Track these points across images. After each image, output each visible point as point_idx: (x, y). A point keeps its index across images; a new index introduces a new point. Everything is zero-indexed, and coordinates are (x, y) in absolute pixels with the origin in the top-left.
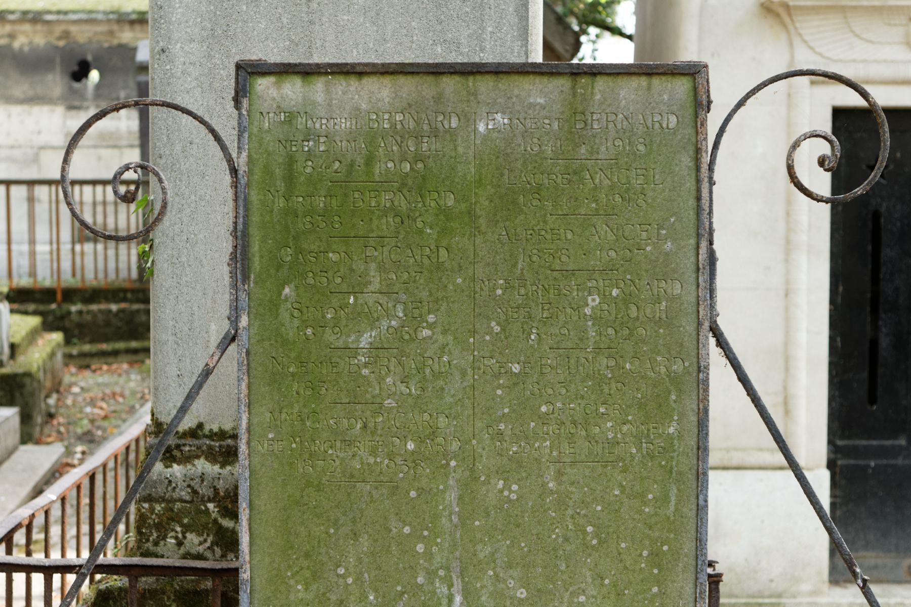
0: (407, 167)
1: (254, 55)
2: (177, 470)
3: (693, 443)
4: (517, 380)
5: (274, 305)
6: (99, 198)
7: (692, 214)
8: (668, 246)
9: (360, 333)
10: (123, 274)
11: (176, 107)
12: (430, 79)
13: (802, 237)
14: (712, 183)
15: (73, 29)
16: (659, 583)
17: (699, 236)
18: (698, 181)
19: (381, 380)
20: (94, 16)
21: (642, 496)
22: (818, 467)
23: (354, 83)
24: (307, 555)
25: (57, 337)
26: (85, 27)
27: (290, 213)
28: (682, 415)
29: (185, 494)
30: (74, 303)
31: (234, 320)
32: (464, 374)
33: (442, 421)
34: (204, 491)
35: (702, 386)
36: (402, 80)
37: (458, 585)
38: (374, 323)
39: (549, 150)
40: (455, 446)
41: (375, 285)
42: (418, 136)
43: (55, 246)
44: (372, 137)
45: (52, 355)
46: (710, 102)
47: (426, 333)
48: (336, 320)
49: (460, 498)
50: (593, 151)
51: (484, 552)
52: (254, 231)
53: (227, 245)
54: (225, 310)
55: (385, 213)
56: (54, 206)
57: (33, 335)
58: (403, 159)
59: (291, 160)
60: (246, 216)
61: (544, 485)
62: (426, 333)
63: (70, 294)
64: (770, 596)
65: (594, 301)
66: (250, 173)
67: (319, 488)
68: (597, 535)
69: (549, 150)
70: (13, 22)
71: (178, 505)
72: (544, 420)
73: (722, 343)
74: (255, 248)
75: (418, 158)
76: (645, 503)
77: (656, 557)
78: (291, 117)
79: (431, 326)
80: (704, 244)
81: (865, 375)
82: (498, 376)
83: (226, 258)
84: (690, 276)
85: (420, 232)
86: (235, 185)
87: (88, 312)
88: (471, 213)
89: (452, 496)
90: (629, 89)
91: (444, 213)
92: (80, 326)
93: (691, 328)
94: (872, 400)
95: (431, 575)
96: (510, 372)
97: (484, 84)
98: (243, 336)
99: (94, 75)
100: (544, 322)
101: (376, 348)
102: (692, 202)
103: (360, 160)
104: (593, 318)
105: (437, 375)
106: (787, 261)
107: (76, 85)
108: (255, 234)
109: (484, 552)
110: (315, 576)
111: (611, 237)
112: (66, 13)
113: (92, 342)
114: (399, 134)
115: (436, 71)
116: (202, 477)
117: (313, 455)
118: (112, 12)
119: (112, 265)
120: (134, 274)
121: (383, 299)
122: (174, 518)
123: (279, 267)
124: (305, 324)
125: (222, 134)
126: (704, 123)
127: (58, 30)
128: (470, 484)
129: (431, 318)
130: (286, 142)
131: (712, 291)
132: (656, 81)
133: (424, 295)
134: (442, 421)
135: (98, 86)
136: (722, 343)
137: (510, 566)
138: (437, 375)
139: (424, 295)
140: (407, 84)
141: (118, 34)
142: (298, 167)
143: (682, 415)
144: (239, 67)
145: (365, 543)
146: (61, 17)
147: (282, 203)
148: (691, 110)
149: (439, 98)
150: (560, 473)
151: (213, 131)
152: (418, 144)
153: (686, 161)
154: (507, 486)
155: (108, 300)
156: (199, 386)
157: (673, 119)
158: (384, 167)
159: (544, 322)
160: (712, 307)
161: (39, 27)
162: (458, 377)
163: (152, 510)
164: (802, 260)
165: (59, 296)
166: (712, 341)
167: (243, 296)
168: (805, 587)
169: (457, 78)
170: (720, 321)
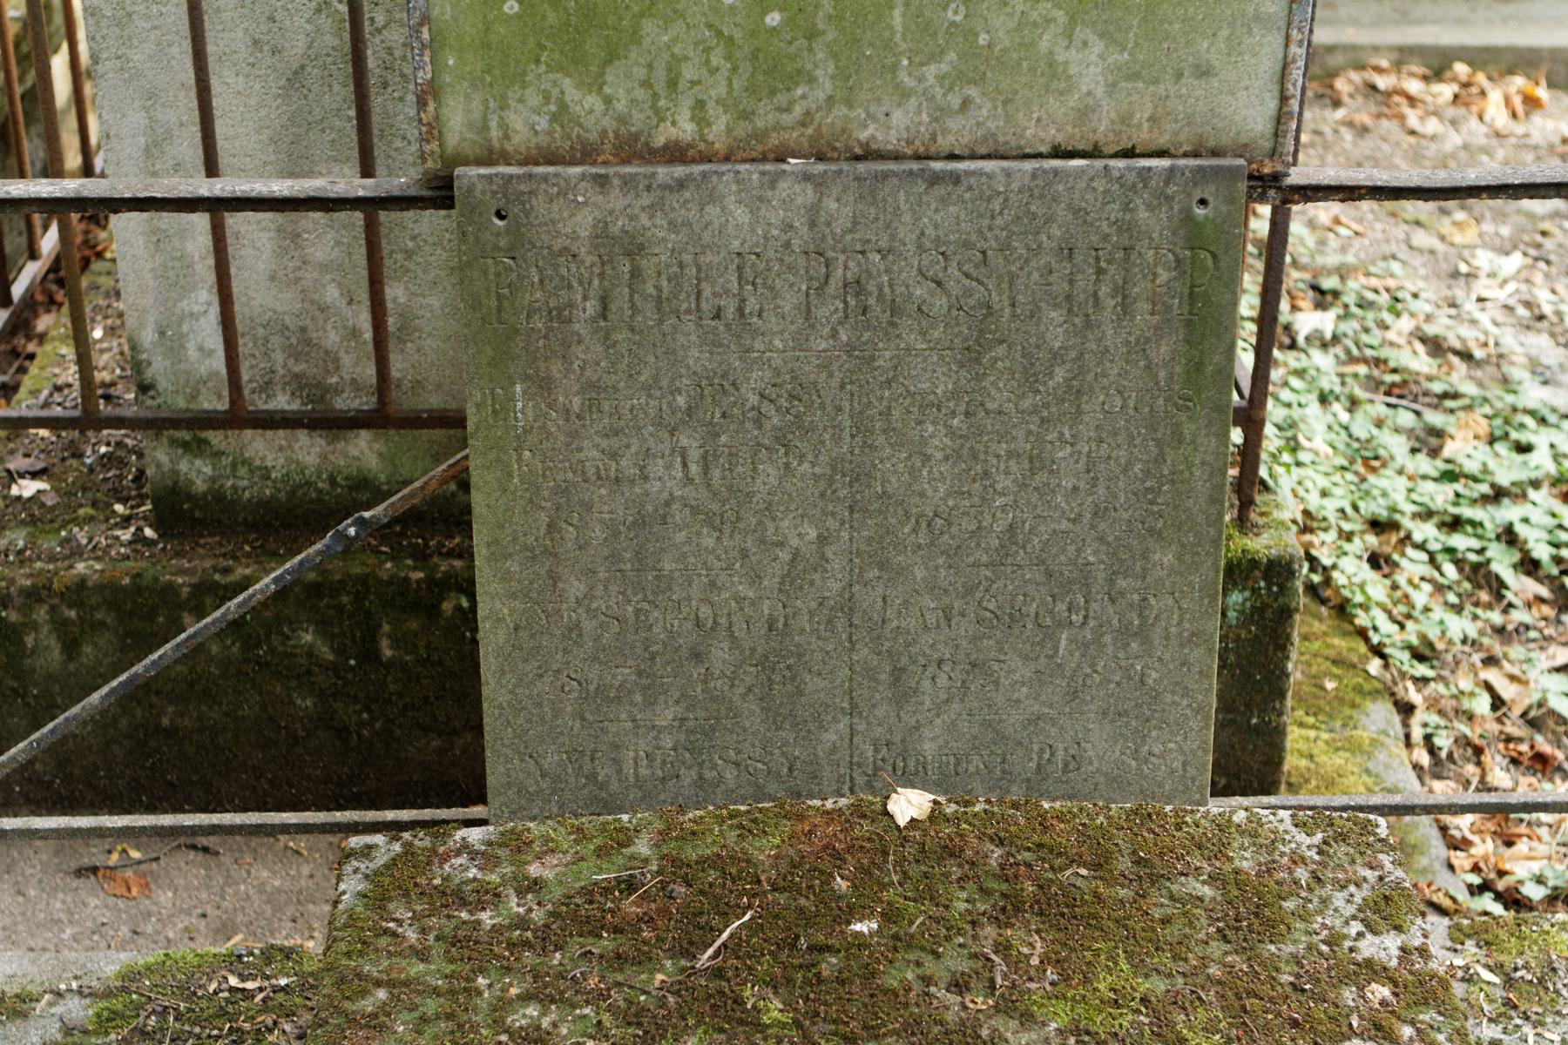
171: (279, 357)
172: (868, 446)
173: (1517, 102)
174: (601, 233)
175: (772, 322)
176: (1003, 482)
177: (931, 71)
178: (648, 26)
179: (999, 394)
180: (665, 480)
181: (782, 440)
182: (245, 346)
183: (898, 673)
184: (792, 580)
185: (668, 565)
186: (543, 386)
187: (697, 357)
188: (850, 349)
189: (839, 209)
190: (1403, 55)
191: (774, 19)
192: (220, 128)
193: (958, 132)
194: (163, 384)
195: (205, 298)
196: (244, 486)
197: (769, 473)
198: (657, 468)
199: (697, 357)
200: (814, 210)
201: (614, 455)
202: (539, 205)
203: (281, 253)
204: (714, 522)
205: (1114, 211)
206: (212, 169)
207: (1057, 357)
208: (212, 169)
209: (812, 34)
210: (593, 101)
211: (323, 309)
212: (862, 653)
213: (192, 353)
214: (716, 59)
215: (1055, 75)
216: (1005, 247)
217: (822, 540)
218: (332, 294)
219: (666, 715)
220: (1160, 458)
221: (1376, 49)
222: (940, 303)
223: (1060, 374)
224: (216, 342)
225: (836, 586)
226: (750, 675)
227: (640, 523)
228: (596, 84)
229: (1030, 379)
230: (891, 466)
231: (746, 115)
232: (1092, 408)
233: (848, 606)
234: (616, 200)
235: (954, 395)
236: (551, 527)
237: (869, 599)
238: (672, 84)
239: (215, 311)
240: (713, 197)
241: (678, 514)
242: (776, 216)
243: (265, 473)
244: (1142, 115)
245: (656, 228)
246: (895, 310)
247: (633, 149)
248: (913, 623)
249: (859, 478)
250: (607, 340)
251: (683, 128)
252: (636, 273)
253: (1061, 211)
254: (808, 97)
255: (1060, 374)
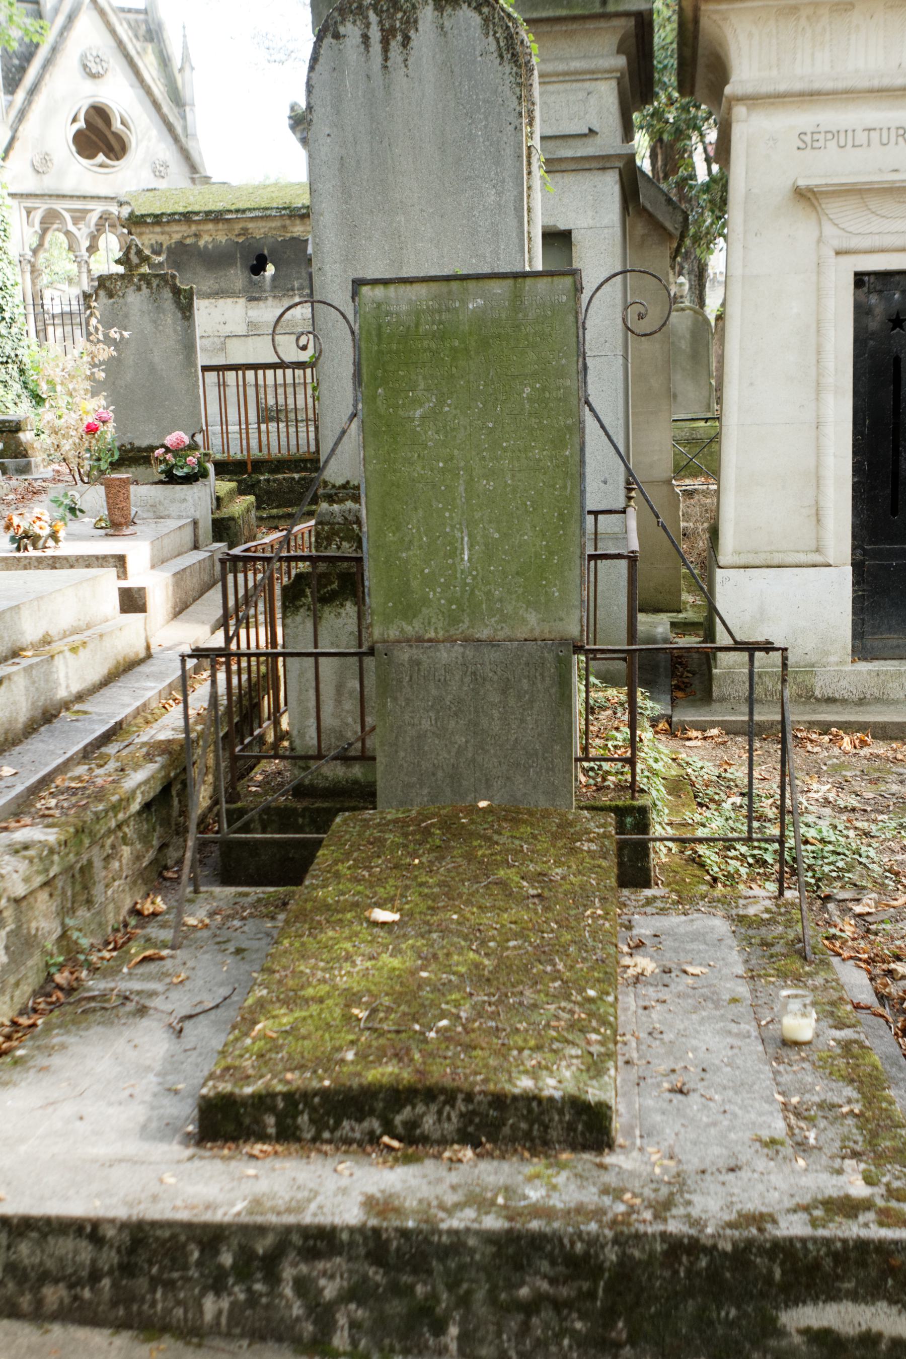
0: (435, 327)
1: (360, 275)
2: (336, 507)
3: (578, 459)
4: (491, 431)
5: (374, 397)
6: (280, 381)
7: (575, 345)
8: (564, 361)
9: (415, 410)
10: (303, 449)
11: (325, 303)
12: (445, 283)
13: (829, 380)
14: (584, 329)
15: (250, 225)
16: (563, 528)
17: (578, 356)
18: (577, 328)
19: (426, 432)
20: (268, 212)
21: (553, 486)
22: (844, 565)
23: (408, 287)
24: (394, 519)
25: (251, 498)
26: (261, 224)
27: (380, 352)
28: (572, 446)
29: (340, 520)
30: (262, 474)
31: (355, 406)
32: (465, 428)
33: (456, 452)
34: (351, 518)
35: (582, 430)
36: (432, 284)
37: (465, 531)
38: (421, 405)
39: (504, 316)
40: (462, 464)
41: (422, 386)
42: (440, 312)
43: (243, 426)
44: (418, 313)
45: (248, 510)
46: (582, 288)
47: (447, 409)
48: (404, 405)
49: (466, 489)
50: (526, 315)
51: (477, 515)
52: (363, 362)
53: (351, 369)
54: (351, 401)
55: (425, 351)
56: (241, 389)
57: (232, 494)
58: (433, 323)
59: (380, 327)
60: (359, 355)
61: (506, 482)
62: (447, 409)
63: (258, 465)
64: (805, 667)
65: (528, 390)
66: (361, 333)
67: (398, 486)
68: (532, 506)
69: (504, 316)
70: (198, 222)
71: (337, 526)
72: (505, 450)
73: (592, 409)
74: (364, 370)
75: (441, 322)
76: (555, 490)
77: (561, 515)
78: (379, 305)
79: (449, 406)
80: (581, 360)
81: (888, 491)
82: (482, 429)
83: (351, 376)
84: (575, 375)
85: (443, 359)
86: (354, 340)
87: (275, 481)
88: (466, 349)
89: (461, 489)
90: (542, 284)
91: (453, 349)
92: (268, 492)
93: (575, 402)
94: (894, 512)
95: (453, 527)
96: (487, 427)
97: (471, 285)
98: (360, 414)
99: (270, 270)
100: (504, 402)
101: (422, 417)
102: (575, 339)
103: (412, 325)
104: (528, 398)
105: (453, 430)
106: (817, 399)
107: (255, 277)
108: (364, 363)
109: (477, 515)
110: (398, 529)
111: (535, 358)
112: (244, 211)
113: (277, 507)
114: (431, 311)
115: (447, 279)
116: (350, 511)
117: (395, 471)
118: (284, 208)
119: (293, 442)
120: (313, 448)
121: (425, 393)
122: (336, 533)
123: (376, 379)
124: (389, 407)
125: (346, 313)
126: (579, 299)
127: (238, 227)
128: (470, 482)
129: (449, 402)
130: (377, 317)
131: (585, 383)
132: (555, 278)
133: (445, 390)
134: (456, 452)
135: (274, 278)
136: (592, 409)
137: (490, 522)
138: (453, 430)
139: (445, 390)
140: (434, 286)
141: (290, 229)
142: (383, 330)
143: (572, 446)
144: (354, 281)
145: (421, 512)
146: (239, 216)
147: (376, 348)
148: (573, 293)
149: (450, 292)
150: (513, 476)
151: (342, 314)
152: (440, 316)
153: (571, 318)
154: (488, 483)
155: (291, 471)
156: (340, 439)
157: (565, 298)
158: (424, 328)
159: (504, 402)
160: (586, 391)
161: (220, 226)
162: (462, 430)
163: (323, 529)
164: (829, 399)
165: (249, 467)
166: (587, 408)
167: (359, 394)
168: (833, 659)
169: (458, 282)
170: (590, 399)
171: (333, 740)
172: (478, 716)
173: (857, 742)
174: (410, 659)
175: (453, 683)
176: (514, 726)
177: (493, 620)
178: (424, 609)
179: (512, 702)
180: (426, 725)
181: (456, 714)
182: (323, 736)
183: (487, 781)
184: (459, 753)
185: (426, 748)
186: (395, 699)
187: (434, 692)
188: (473, 690)
189: (470, 653)
190: (811, 725)
191: (454, 607)
192: (320, 669)
193: (501, 635)
194: (298, 748)
195: (312, 721)
196: (321, 783)
197: (452, 723)
198: (423, 722)
199: (434, 692)
200: (463, 653)
201: (412, 718)
202: (395, 652)
203: (336, 707)
204: (438, 736)
205: (539, 653)
206: (316, 647)
207: (526, 692)
208: (316, 647)
209: (463, 611)
210: (410, 628)
211: (347, 724)
212: (478, 774)
213: (307, 738)
214: (440, 617)
215: (524, 621)
216: (511, 663)
217: (467, 742)
218: (350, 720)
219: (425, 791)
220: (554, 720)
221: (799, 722)
222: (496, 678)
223: (527, 697)
224: (315, 735)
225: (470, 755)
226: (448, 780)
227: (419, 737)
228: (411, 623)
229: (519, 697)
230: (484, 722)
231: (447, 631)
232: (536, 705)
233: (473, 760)
234: (414, 651)
235: (500, 702)
236: (396, 737)
237: (479, 759)
238: (429, 623)
239: (315, 726)
240: (439, 650)
241: (429, 734)
242: (454, 655)
243: (326, 778)
244: (546, 631)
245: (424, 658)
246: (484, 679)
247: (420, 640)
248: (490, 765)
249: (476, 724)
250: (411, 687)
251: (432, 634)
252: (419, 670)
253: (526, 654)
254: (463, 626)
255: (527, 697)
